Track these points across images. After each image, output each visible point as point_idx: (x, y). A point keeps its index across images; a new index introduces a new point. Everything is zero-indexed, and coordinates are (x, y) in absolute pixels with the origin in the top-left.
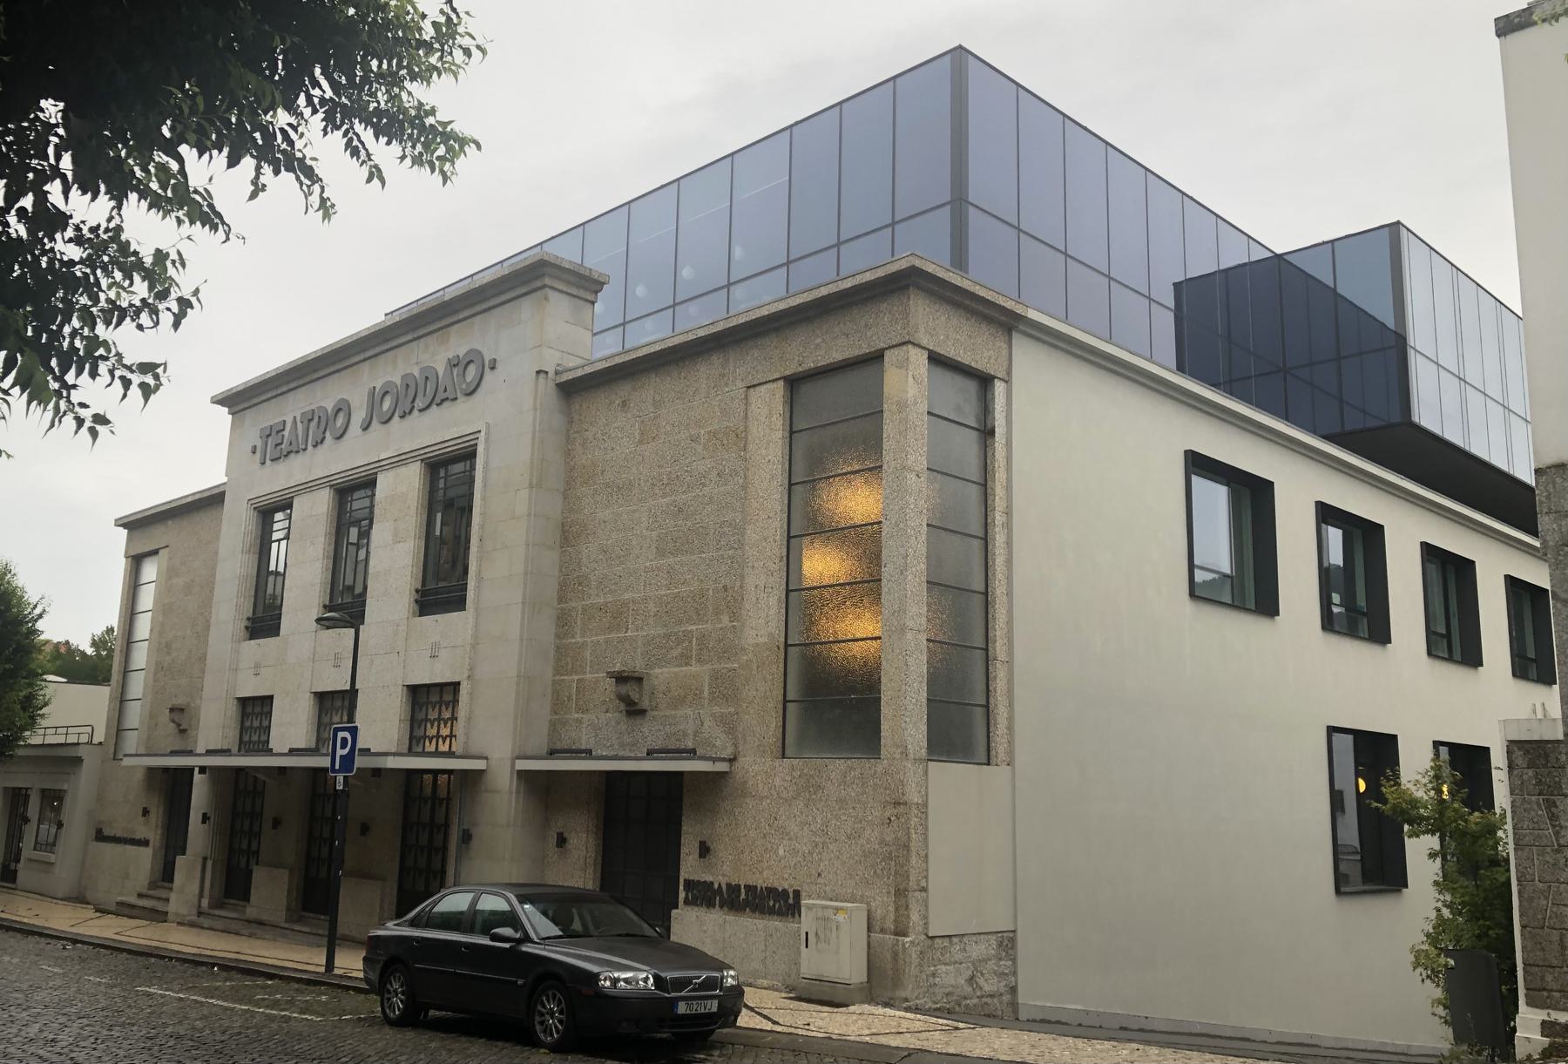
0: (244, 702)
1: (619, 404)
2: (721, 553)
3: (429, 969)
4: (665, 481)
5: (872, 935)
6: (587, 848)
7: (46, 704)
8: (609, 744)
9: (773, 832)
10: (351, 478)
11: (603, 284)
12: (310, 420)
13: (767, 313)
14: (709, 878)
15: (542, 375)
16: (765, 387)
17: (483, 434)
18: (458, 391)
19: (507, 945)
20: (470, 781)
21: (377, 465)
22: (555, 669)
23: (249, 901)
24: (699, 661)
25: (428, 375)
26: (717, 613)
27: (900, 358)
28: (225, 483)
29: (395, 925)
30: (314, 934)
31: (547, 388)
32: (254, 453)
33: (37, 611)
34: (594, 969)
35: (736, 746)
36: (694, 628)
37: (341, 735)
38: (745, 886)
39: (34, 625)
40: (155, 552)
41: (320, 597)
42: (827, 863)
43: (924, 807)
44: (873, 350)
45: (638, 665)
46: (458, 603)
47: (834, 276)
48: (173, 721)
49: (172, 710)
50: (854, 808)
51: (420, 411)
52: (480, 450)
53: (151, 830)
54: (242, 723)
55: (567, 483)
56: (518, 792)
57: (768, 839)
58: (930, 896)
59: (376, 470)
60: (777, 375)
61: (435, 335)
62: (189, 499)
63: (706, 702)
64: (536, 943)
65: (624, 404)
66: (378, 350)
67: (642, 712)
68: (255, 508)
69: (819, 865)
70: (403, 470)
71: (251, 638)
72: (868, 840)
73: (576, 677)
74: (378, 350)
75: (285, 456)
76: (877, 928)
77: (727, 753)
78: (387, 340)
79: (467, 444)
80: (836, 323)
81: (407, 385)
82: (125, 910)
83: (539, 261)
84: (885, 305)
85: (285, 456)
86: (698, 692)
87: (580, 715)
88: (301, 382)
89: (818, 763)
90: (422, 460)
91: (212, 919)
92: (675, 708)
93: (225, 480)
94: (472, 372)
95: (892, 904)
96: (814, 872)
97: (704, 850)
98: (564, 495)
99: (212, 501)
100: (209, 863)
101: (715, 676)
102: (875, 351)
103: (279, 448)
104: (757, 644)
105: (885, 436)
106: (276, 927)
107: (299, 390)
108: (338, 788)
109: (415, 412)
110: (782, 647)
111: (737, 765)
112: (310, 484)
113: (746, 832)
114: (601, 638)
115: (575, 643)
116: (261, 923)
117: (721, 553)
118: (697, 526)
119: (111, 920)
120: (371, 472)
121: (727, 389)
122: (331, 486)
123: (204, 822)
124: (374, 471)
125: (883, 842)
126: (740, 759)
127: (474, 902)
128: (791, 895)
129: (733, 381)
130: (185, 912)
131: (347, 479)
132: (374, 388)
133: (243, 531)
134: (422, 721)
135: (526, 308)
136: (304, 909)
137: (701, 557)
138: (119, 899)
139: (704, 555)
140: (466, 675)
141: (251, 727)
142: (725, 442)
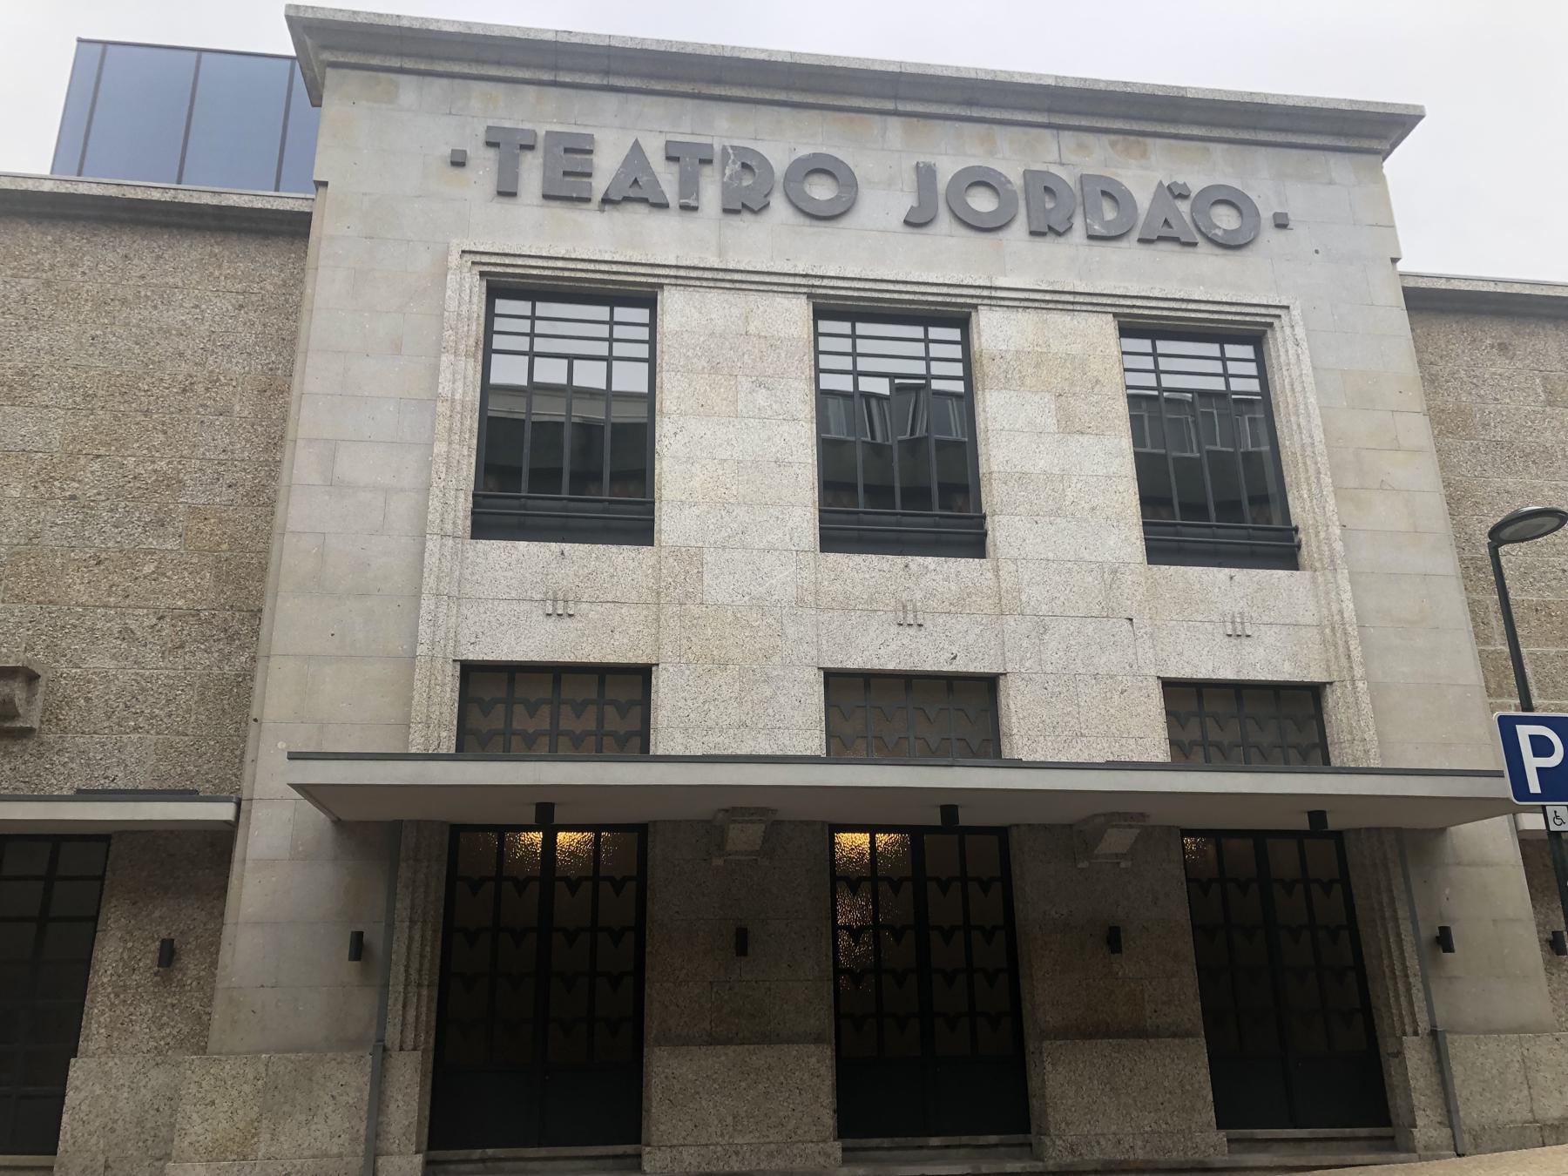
10: (888, 296)
21: (986, 293)
59: (979, 301)
68: (482, 274)
78: (970, 103)
120: (969, 301)
124: (974, 301)
131: (567, 274)
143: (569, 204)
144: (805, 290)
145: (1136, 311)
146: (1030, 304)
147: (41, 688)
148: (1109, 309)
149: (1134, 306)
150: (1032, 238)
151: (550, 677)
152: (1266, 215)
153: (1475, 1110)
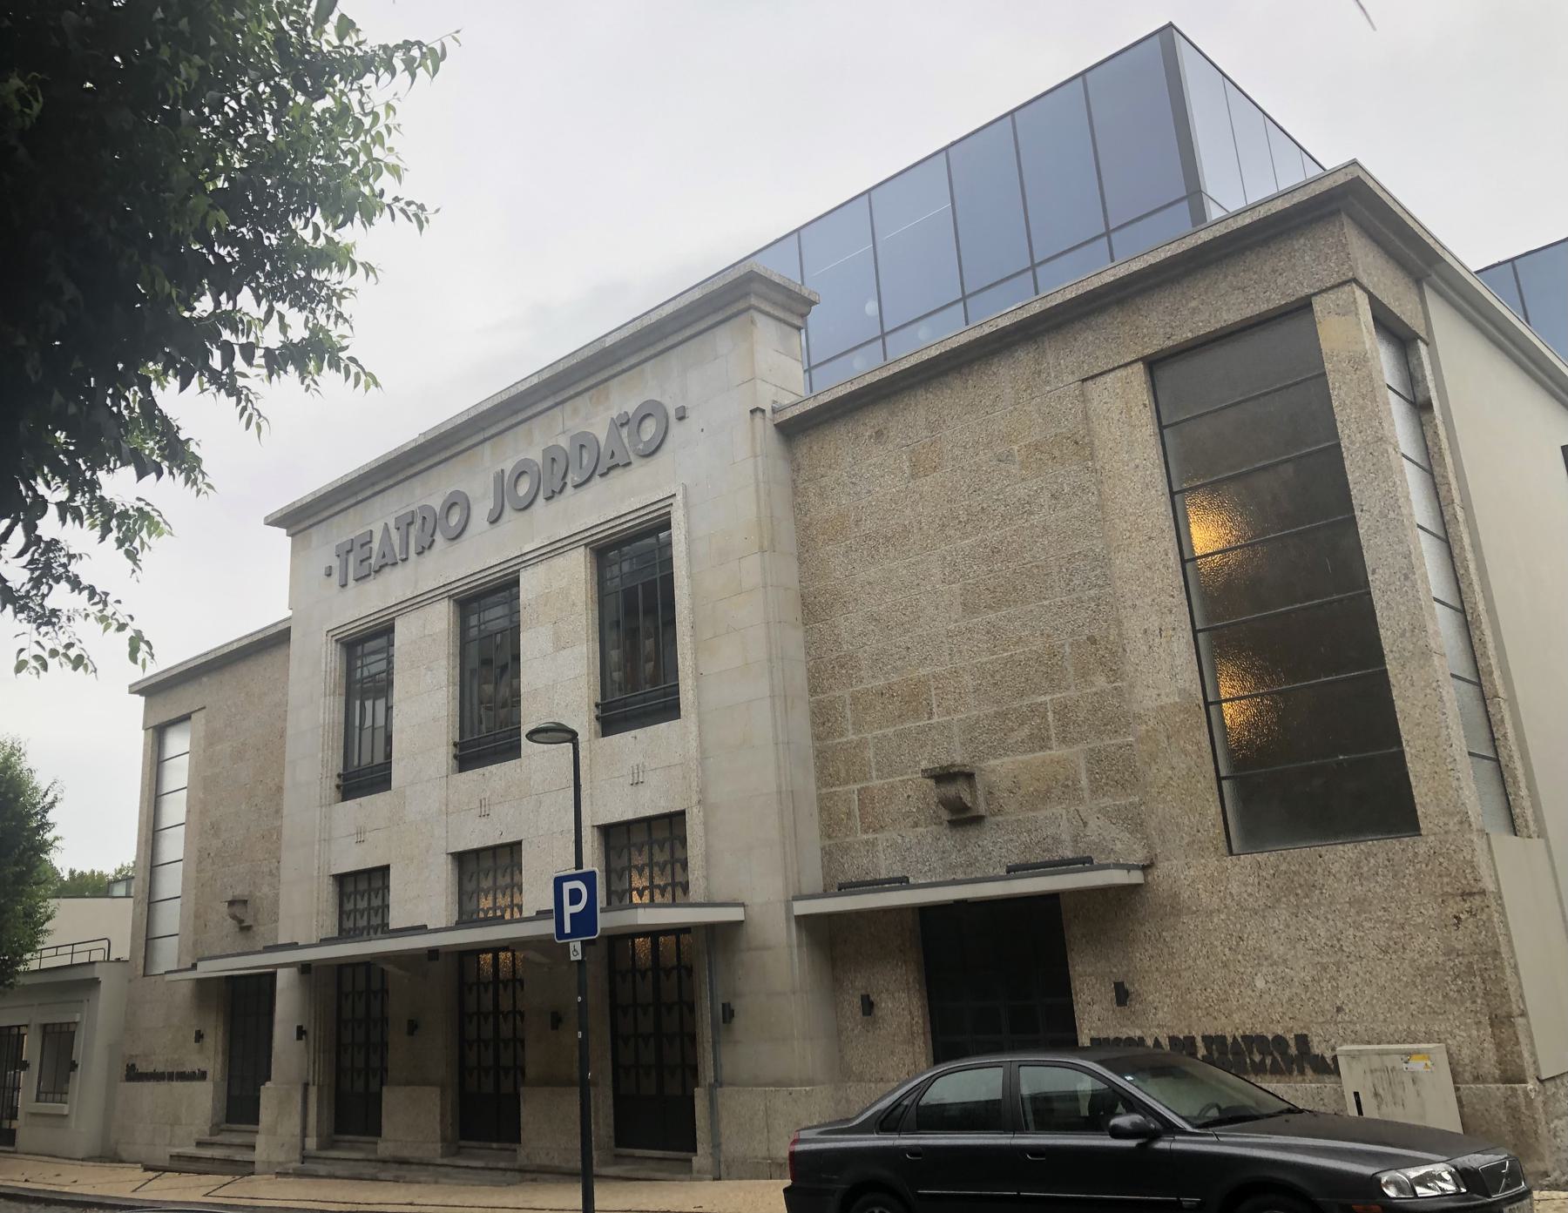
0: (341, 879)
1: (870, 437)
2: (1074, 596)
3: (949, 1195)
4: (964, 518)
5: (1462, 1086)
6: (910, 1013)
7: (49, 918)
8: (926, 868)
9: (1240, 957)
10: (479, 582)
11: (813, 303)
12: (409, 524)
13: (1112, 279)
14: (1136, 1033)
15: (759, 414)
16: (1111, 375)
17: (679, 497)
18: (631, 453)
19: (1131, 1143)
20: (721, 937)
21: (520, 560)
22: (818, 780)
23: (379, 1135)
24: (1064, 741)
25: (583, 443)
26: (1084, 674)
27: (1341, 302)
28: (290, 618)
29: (821, 1133)
30: (491, 1169)
31: (765, 429)
32: (329, 575)
33: (49, 799)
34: (1368, 1170)
35: (1150, 847)
36: (1048, 698)
37: (567, 886)
38: (1204, 1038)
39: (43, 817)
40: (186, 718)
41: (448, 733)
42: (1351, 991)
43: (1499, 896)
44: (1293, 299)
45: (958, 757)
46: (669, 709)
47: (882, 362)
48: (234, 917)
49: (231, 903)
50: (1385, 909)
51: (576, 487)
52: (677, 518)
53: (210, 1059)
54: (341, 905)
55: (803, 544)
56: (799, 946)
57: (1232, 968)
58: (1531, 1021)
60: (1133, 357)
61: (587, 395)
62: (235, 646)
63: (1086, 794)
64: (1184, 1132)
65: (879, 434)
66: (501, 426)
67: (978, 820)
68: (337, 641)
69: (1337, 996)
70: (559, 562)
71: (344, 799)
72: (1422, 953)
73: (856, 787)
74: (501, 426)
75: (376, 572)
76: (1467, 1076)
77: (1139, 857)
78: (516, 412)
79: (655, 514)
80: (1221, 277)
81: (553, 459)
82: (182, 1164)
83: (746, 274)
84: (1302, 241)
85: (376, 572)
86: (1070, 783)
87: (870, 836)
88: (391, 482)
89: (1304, 855)
90: (586, 545)
91: (325, 1164)
92: (1034, 808)
93: (290, 613)
94: (649, 429)
95: (1488, 1039)
96: (1327, 1007)
97: (1122, 995)
98: (798, 559)
99: (275, 641)
100: (313, 1091)
101: (1096, 759)
102: (1297, 300)
103: (365, 563)
104: (1162, 707)
105: (1335, 404)
106: (428, 1164)
107: (390, 492)
108: (573, 958)
109: (569, 489)
110: (1202, 705)
111: (1157, 873)
112: (419, 599)
113: (1190, 962)
114: (890, 731)
115: (847, 742)
116: (403, 1162)
117: (1074, 596)
118: (1029, 566)
119: (170, 1179)
121: (1048, 388)
122: (450, 597)
123: (299, 1038)
125: (1450, 952)
126: (1160, 865)
127: (1011, 1084)
128: (1292, 1043)
129: (1056, 377)
130: (282, 1158)
131: (650, 516)
132: (502, 471)
133: (324, 669)
134: (623, 870)
135: (723, 340)
136: (463, 1138)
137: (1043, 606)
138: (176, 1151)
139: (1046, 603)
140: (695, 799)
141: (355, 910)
142: (1057, 453)
143: (363, 581)
144: (446, 595)
145: (595, 538)
146: (544, 557)
147: (977, 779)
148: (581, 543)
149: (593, 535)
150: (604, 478)
151: (667, 820)
152: (672, 414)
153: (733, 1146)
